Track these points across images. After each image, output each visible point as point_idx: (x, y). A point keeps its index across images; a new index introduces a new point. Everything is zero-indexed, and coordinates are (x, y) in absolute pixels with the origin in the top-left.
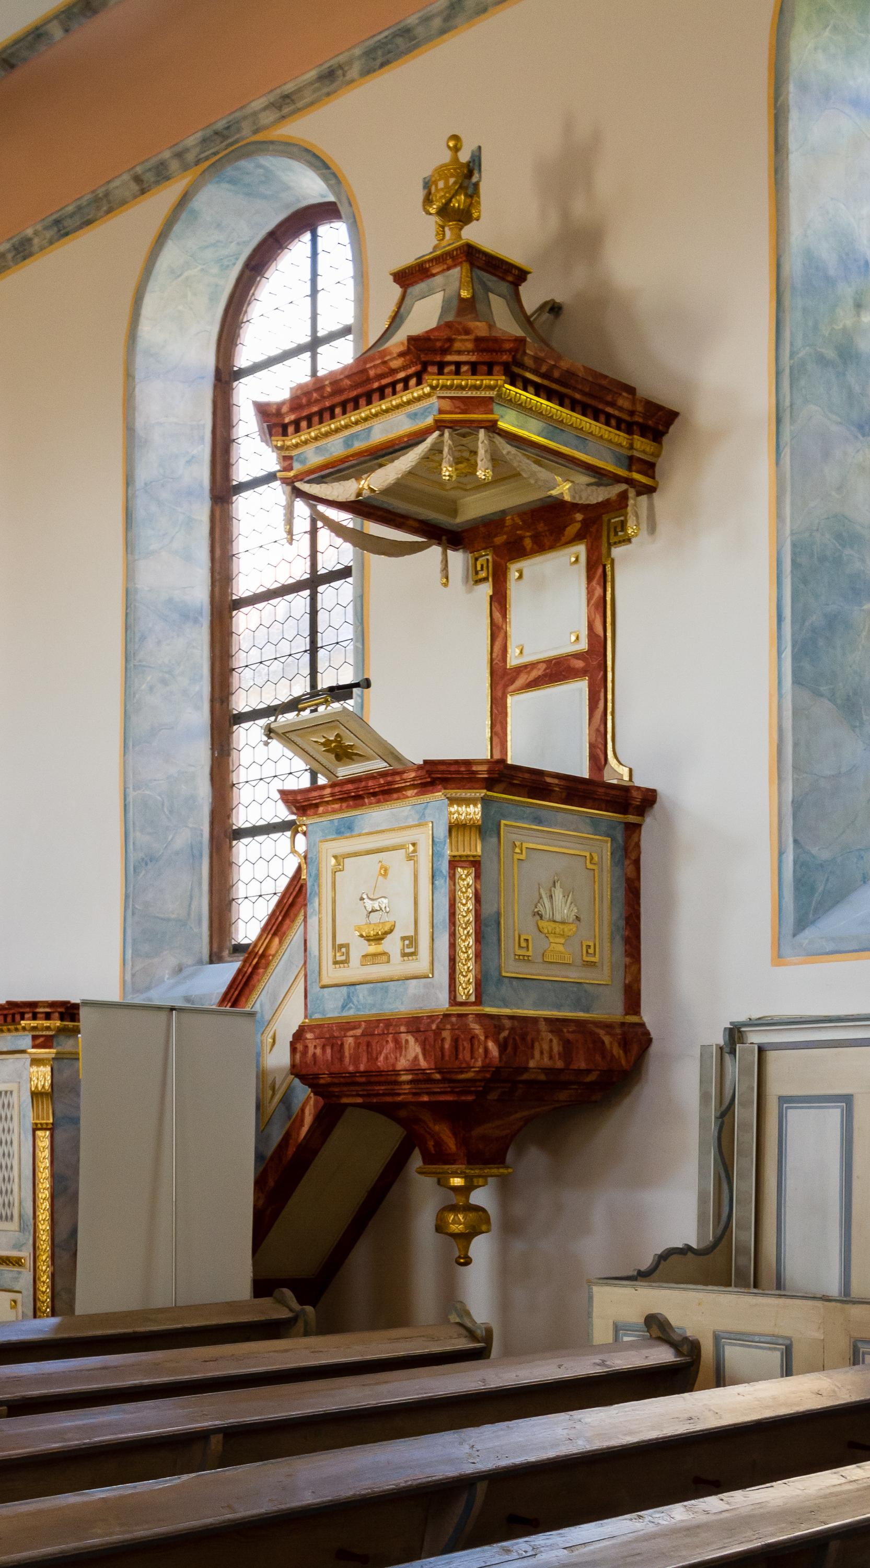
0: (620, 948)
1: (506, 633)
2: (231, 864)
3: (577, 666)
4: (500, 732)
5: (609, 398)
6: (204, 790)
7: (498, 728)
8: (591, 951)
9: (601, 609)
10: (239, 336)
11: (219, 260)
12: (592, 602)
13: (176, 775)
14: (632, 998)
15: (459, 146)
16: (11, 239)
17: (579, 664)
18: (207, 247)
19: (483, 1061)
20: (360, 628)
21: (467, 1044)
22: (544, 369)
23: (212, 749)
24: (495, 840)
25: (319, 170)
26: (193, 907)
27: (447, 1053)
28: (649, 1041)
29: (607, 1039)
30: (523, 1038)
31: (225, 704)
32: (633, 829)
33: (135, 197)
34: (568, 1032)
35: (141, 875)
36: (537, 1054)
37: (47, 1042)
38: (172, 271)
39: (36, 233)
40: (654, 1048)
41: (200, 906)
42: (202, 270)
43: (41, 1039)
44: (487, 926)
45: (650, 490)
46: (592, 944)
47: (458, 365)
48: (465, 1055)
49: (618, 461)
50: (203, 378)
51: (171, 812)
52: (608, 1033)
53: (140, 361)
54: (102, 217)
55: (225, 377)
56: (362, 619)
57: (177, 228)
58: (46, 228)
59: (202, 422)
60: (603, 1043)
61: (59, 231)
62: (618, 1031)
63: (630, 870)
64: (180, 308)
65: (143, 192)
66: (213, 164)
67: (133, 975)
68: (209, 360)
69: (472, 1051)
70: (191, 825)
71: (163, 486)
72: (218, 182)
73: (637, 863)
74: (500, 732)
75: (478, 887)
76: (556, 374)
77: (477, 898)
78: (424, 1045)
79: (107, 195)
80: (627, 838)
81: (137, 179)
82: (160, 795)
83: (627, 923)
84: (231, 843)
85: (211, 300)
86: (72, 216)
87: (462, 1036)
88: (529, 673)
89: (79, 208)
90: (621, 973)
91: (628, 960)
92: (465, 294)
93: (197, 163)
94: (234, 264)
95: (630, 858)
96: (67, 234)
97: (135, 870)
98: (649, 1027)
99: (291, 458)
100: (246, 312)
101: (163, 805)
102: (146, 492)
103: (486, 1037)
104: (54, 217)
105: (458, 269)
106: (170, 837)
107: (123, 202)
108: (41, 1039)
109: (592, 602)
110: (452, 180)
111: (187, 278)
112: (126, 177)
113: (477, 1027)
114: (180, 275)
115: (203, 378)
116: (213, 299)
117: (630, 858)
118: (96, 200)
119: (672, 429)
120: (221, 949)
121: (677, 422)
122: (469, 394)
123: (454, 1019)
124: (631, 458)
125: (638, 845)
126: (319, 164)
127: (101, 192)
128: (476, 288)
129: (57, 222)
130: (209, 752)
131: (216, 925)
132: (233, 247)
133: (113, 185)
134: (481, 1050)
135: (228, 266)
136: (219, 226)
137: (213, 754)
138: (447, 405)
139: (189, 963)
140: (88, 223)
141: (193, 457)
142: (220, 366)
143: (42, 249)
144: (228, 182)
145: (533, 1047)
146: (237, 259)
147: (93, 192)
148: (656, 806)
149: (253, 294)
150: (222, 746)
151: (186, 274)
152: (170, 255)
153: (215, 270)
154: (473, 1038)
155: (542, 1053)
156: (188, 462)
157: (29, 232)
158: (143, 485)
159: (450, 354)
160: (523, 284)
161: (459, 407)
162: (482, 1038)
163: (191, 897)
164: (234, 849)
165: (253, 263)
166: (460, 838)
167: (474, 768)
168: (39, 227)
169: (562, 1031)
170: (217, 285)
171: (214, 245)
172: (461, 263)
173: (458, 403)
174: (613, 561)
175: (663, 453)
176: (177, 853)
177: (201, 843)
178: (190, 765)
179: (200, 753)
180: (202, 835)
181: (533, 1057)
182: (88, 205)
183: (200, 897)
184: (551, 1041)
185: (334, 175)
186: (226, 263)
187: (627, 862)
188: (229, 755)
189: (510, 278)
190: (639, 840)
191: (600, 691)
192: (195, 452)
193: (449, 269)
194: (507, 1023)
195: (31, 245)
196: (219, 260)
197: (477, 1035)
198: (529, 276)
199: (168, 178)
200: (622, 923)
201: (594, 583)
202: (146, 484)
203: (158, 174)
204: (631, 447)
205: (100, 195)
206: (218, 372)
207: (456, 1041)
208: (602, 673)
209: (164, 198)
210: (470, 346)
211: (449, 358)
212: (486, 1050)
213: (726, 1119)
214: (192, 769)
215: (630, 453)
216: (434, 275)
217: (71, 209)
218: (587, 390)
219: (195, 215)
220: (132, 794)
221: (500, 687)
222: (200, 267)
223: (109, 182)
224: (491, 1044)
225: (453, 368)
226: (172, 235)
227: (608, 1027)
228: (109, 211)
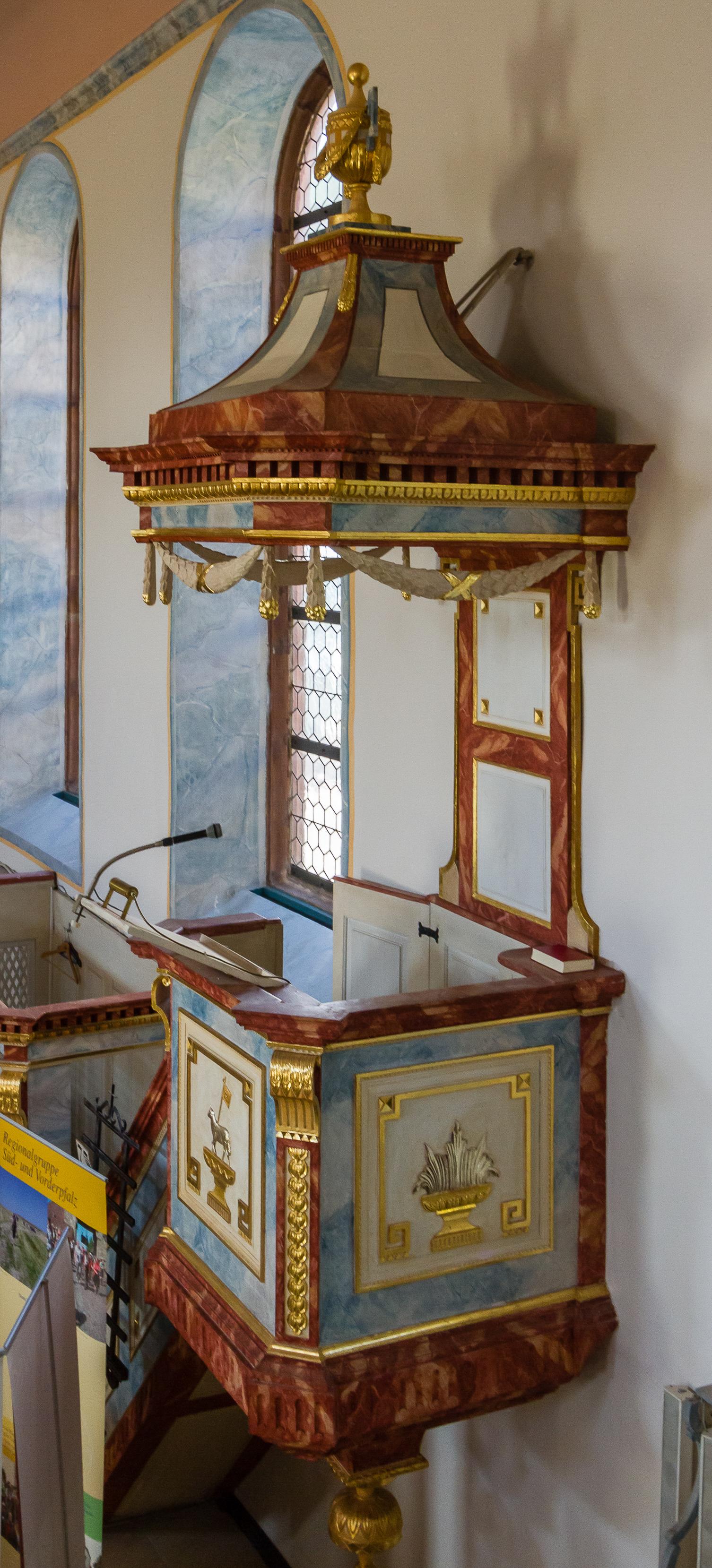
0: (571, 1192)
1: (472, 676)
2: (289, 774)
3: (540, 757)
4: (465, 799)
5: (532, 453)
6: (260, 692)
7: (464, 796)
8: (518, 1214)
9: (565, 692)
10: (298, 178)
11: (266, 104)
12: (556, 679)
13: (227, 679)
14: (591, 1261)
15: (362, 77)
16: (92, 75)
17: (542, 756)
18: (247, 93)
19: (312, 1437)
20: (346, 603)
21: (291, 1409)
22: (408, 447)
23: (270, 645)
24: (346, 1103)
25: (315, 32)
26: (247, 823)
27: (266, 1417)
28: (614, 1326)
29: (537, 1342)
30: (385, 1383)
31: (284, 594)
32: (592, 1029)
33: (121, 81)
34: (470, 1349)
35: (187, 793)
36: (410, 1399)
37: (20, 1055)
38: (213, 123)
39: (108, 70)
40: (621, 1336)
41: (256, 822)
42: (247, 116)
43: (14, 1050)
44: (329, 1229)
45: (622, 549)
46: (519, 1204)
47: (274, 465)
48: (290, 1423)
49: (563, 522)
50: (259, 230)
51: (220, 721)
52: (542, 1331)
53: (184, 221)
54: (155, 59)
55: (284, 226)
56: (349, 592)
57: (207, 81)
58: (115, 66)
59: (258, 280)
60: (532, 1348)
61: (126, 70)
62: (560, 1321)
63: (590, 1083)
64: (228, 158)
65: (181, 37)
66: (232, 13)
67: (177, 904)
68: (267, 208)
69: (299, 1419)
70: (244, 733)
71: (212, 359)
72: (239, 32)
73: (600, 1071)
74: (465, 799)
75: (316, 1179)
76: (432, 448)
77: (315, 1197)
78: (246, 1379)
79: (154, 38)
80: (584, 1037)
81: (175, 24)
82: (208, 704)
83: (582, 1158)
84: (289, 751)
85: (263, 144)
86: (132, 55)
87: (285, 1396)
88: (493, 740)
89: (136, 49)
90: (574, 1226)
91: (583, 1209)
92: (341, 306)
93: (220, 10)
94: (284, 105)
95: (588, 1066)
96: (131, 74)
97: (178, 788)
98: (615, 1302)
99: (149, 510)
100: (304, 152)
101: (212, 715)
102: (192, 368)
103: (317, 1403)
104: (119, 56)
105: (341, 263)
106: (219, 750)
107: (168, 47)
108: (14, 1050)
109: (556, 679)
110: (344, 134)
111: (232, 127)
112: (165, 22)
113: (305, 1386)
114: (222, 126)
115: (259, 230)
116: (265, 143)
117: (588, 1066)
118: (147, 42)
119: (647, 466)
120: (279, 866)
121: (653, 457)
122: (293, 499)
123: (277, 1367)
124: (584, 513)
125: (602, 1044)
126: (314, 24)
127: (148, 35)
128: (363, 290)
129: (122, 61)
130: (267, 649)
131: (273, 841)
132: (277, 89)
133: (156, 29)
134: (310, 1421)
135: (276, 108)
136: (255, 71)
137: (271, 651)
138: (264, 514)
139: (243, 885)
140: (145, 64)
141: (248, 321)
142: (280, 214)
143: (116, 86)
144: (250, 30)
145: (403, 1389)
146: (286, 99)
147: (143, 34)
148: (625, 996)
149: (310, 133)
150: (281, 642)
151: (230, 123)
152: (209, 106)
153: (263, 114)
154: (299, 1404)
155: (419, 1393)
156: (242, 328)
157: (103, 69)
158: (188, 361)
159: (259, 451)
160: (449, 259)
161: (281, 518)
162: (312, 1404)
163: (245, 812)
164: (293, 758)
165: (305, 101)
166: (292, 1110)
167: (299, 1027)
168: (109, 65)
169: (458, 1352)
170: (267, 129)
171: (254, 90)
172: (346, 254)
173: (279, 511)
174: (579, 629)
175: (637, 497)
176: (228, 766)
177: (256, 751)
178: (243, 666)
179: (258, 649)
180: (257, 743)
181: (402, 1406)
182: (142, 46)
183: (256, 810)
184: (437, 1372)
185: (327, 39)
186: (273, 105)
187: (584, 1071)
188: (288, 652)
189: (428, 257)
190: (605, 1035)
191: (563, 804)
192: (251, 314)
193: (336, 258)
194: (360, 1366)
195: (108, 81)
196: (266, 104)
197: (304, 1398)
198: (457, 247)
199: (198, 25)
200: (576, 1156)
201: (558, 653)
202: (192, 360)
203: (191, 20)
204: (581, 500)
205: (149, 39)
206: (277, 221)
207: (277, 1401)
208: (565, 781)
209: (189, 54)
210: (282, 443)
211: (257, 457)
212: (317, 1421)
213: (683, 1543)
214: (247, 670)
215: (582, 507)
216: (323, 263)
217: (129, 49)
218: (491, 453)
219: (225, 66)
220: (176, 705)
221: (466, 743)
222: (244, 114)
223: (153, 26)
224: (323, 1414)
225: (268, 466)
226: (205, 88)
227: (541, 1319)
228: (159, 54)
